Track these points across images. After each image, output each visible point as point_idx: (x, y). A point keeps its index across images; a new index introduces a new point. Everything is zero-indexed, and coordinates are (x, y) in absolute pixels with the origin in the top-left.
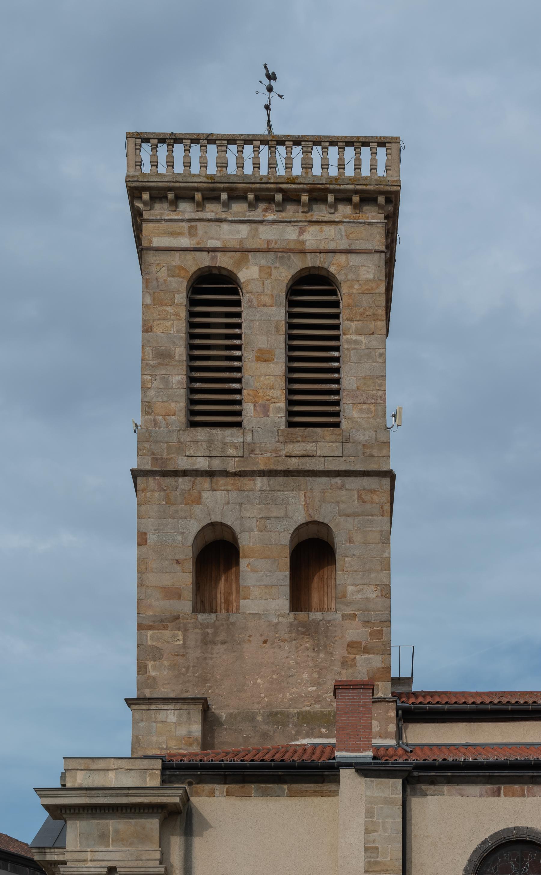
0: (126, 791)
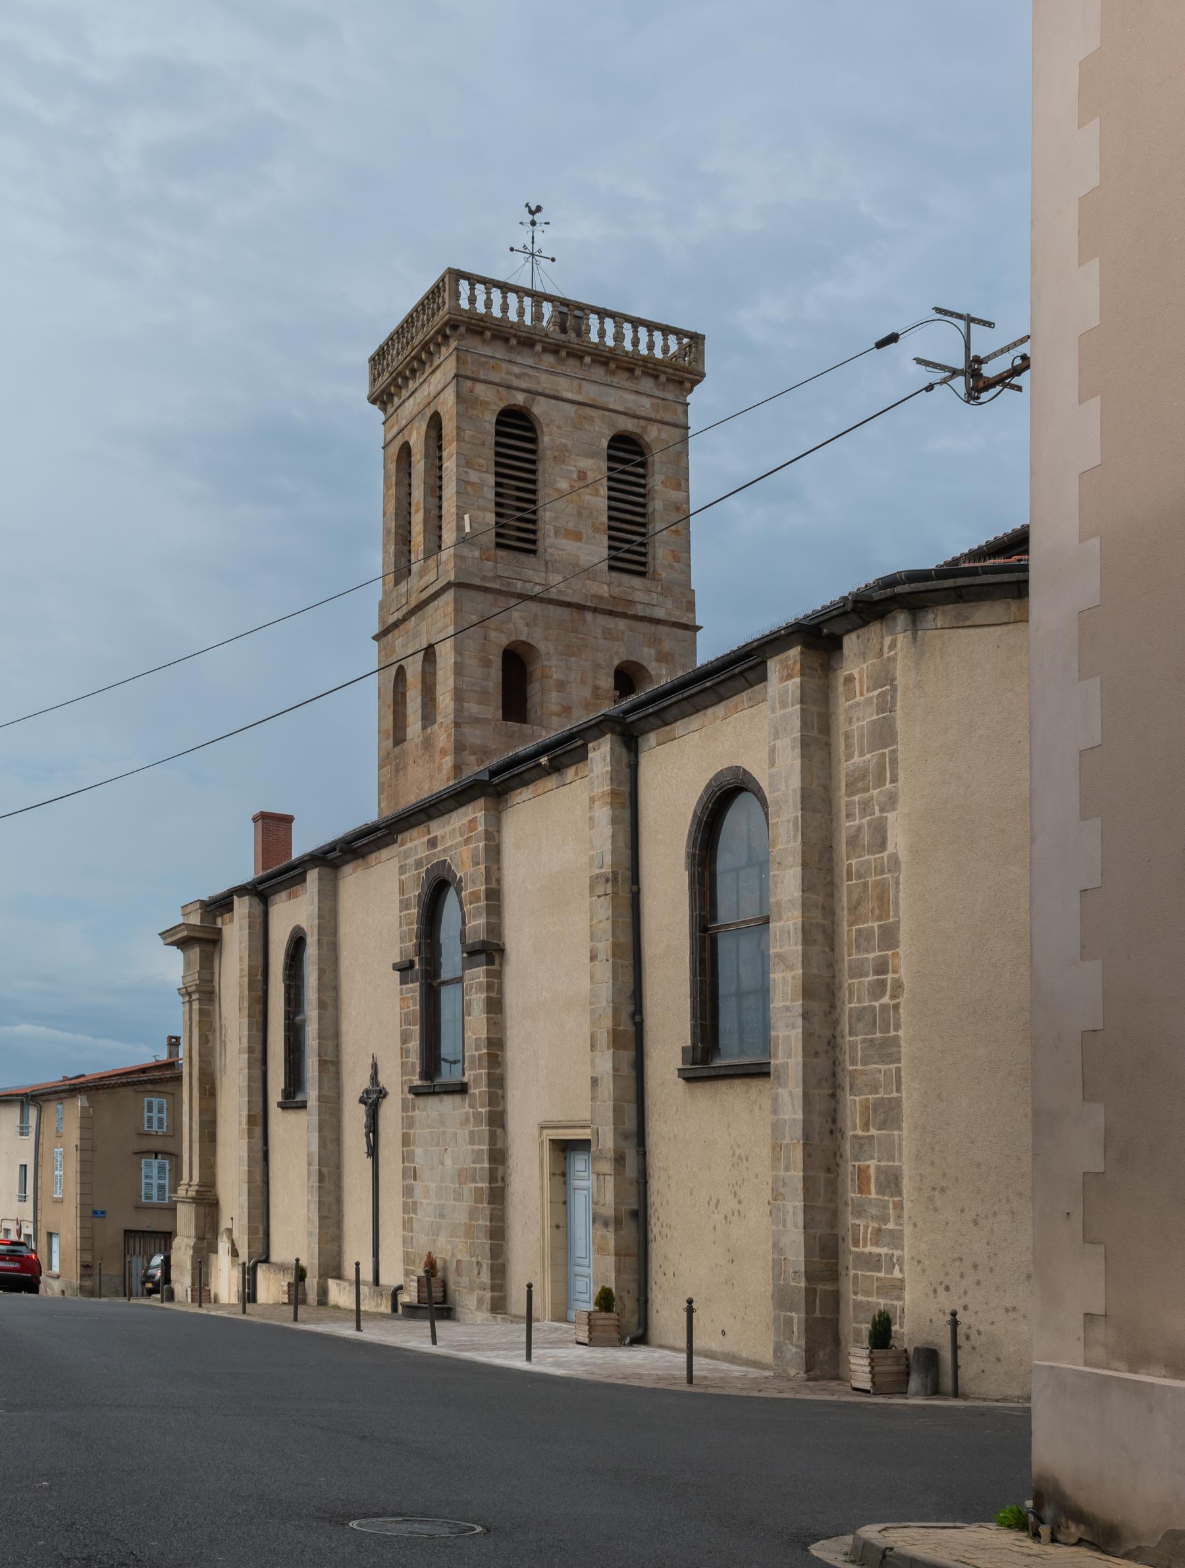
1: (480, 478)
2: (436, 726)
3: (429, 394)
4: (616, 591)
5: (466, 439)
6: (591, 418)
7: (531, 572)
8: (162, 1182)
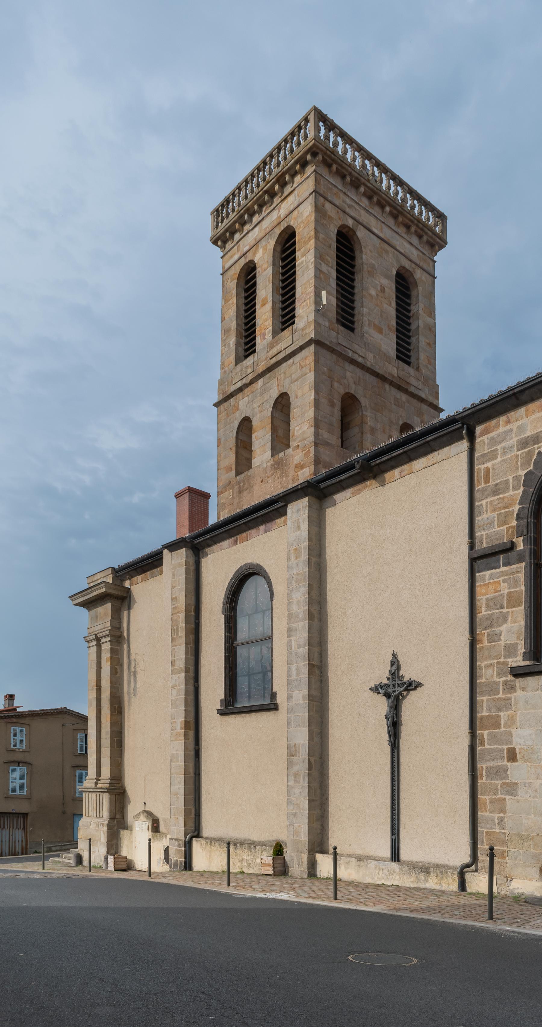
0: (90, 590)
1: (328, 271)
2: (290, 450)
3: (279, 217)
4: (402, 374)
5: (320, 239)
6: (387, 252)
7: (357, 347)
8: (22, 781)
